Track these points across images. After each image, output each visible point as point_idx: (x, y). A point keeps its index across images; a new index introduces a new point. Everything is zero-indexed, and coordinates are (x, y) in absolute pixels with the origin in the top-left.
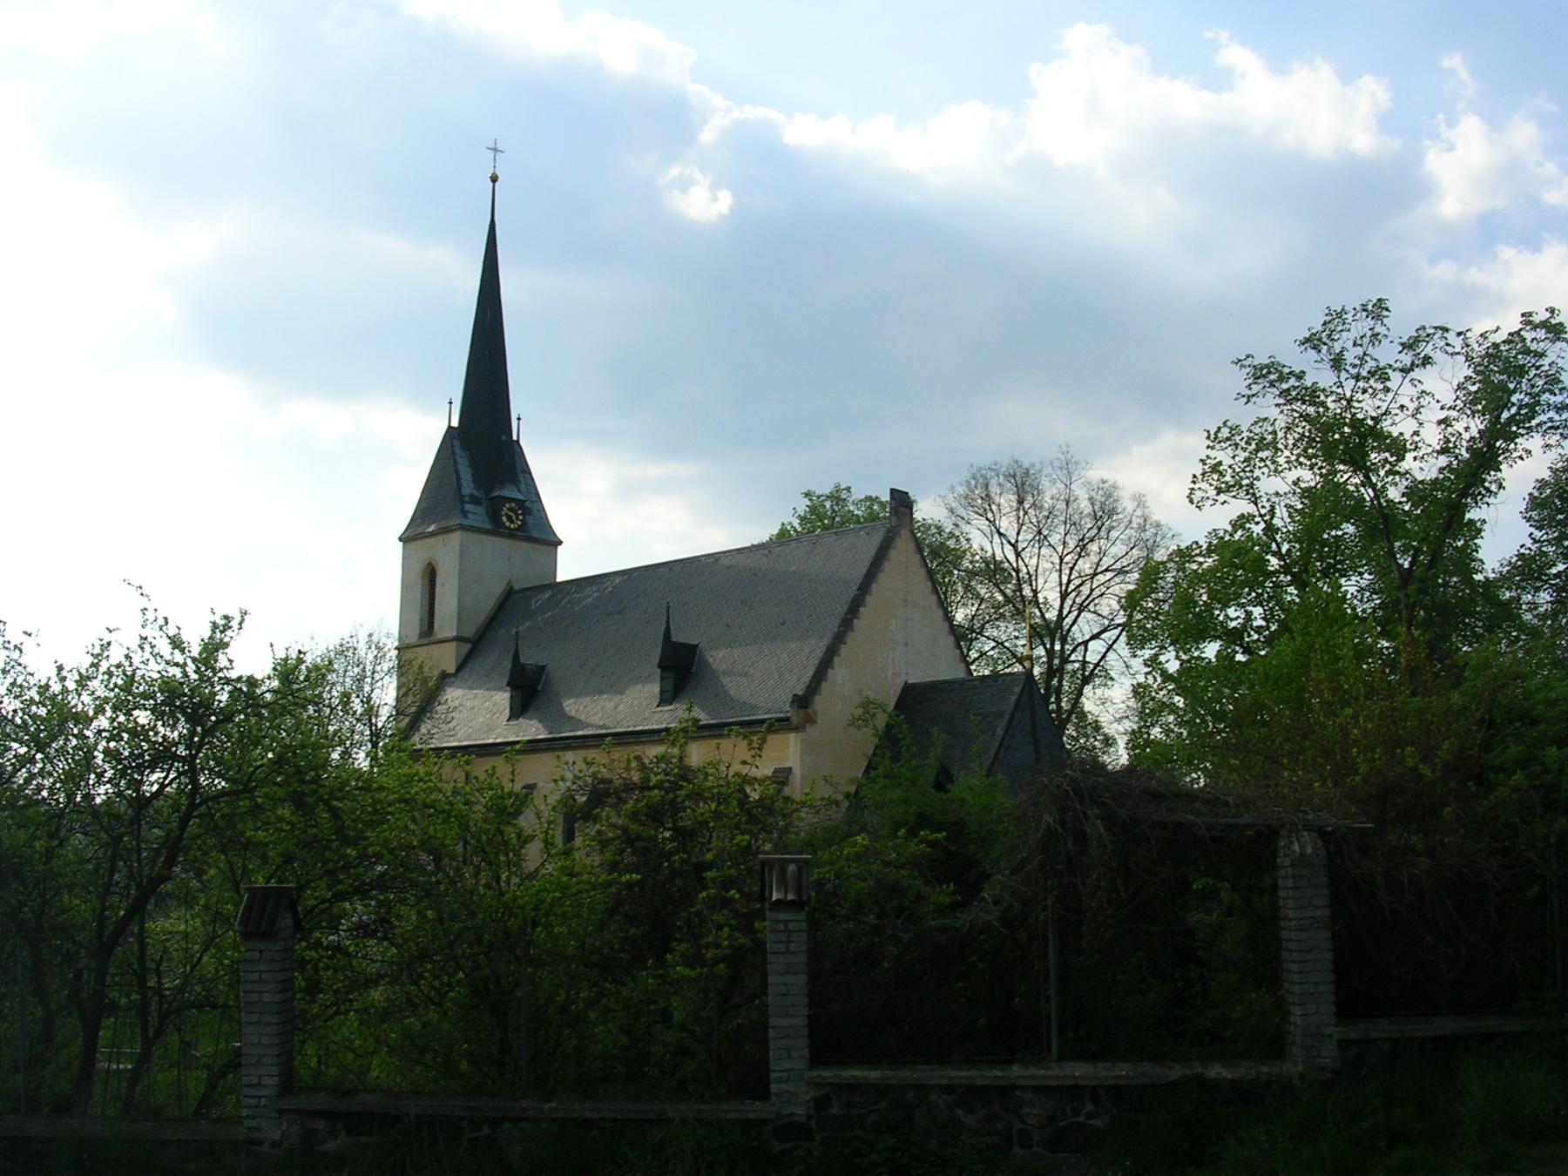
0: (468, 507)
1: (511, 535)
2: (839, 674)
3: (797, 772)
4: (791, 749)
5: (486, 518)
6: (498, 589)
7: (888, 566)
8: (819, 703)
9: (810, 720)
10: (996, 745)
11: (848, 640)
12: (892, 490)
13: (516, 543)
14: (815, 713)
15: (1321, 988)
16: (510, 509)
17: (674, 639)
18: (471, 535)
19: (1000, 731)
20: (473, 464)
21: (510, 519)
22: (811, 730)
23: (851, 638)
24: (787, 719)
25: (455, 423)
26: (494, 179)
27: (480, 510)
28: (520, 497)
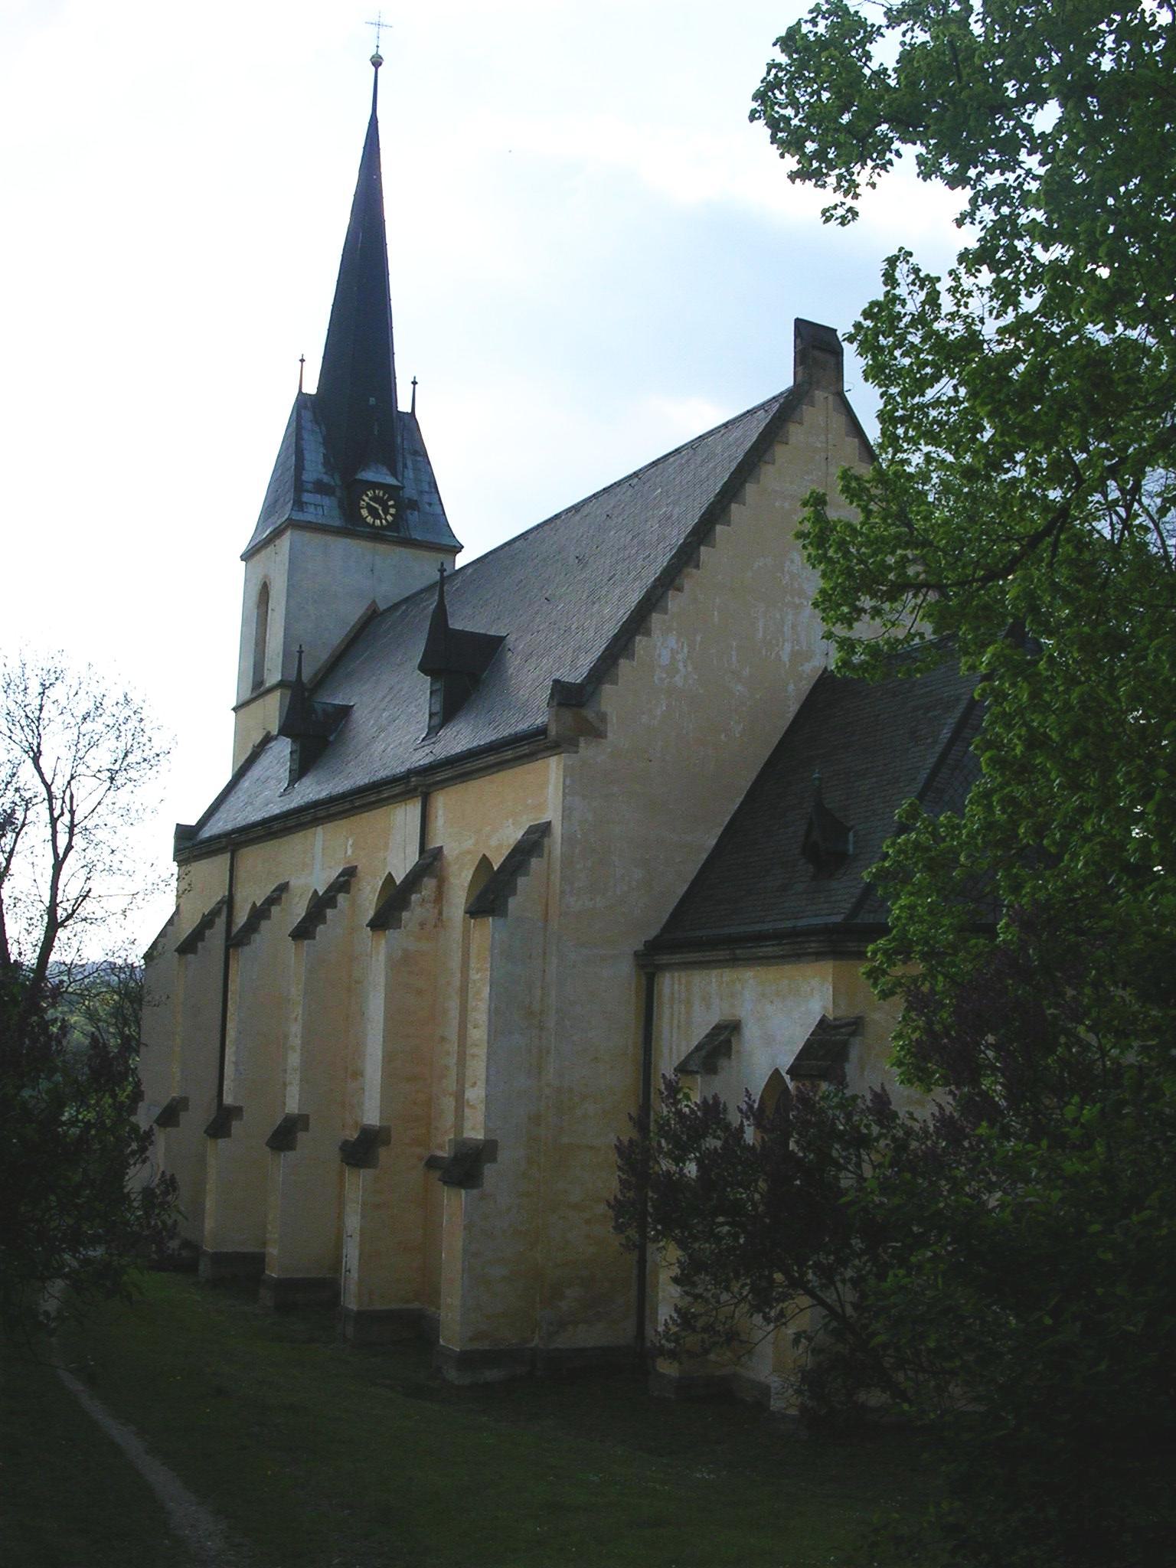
0: (307, 497)
1: (376, 535)
2: (663, 645)
3: (557, 829)
4: (551, 788)
5: (336, 512)
6: (354, 612)
7: (781, 452)
8: (611, 700)
9: (595, 732)
10: (932, 760)
11: (687, 584)
12: (799, 323)
13: (382, 548)
14: (603, 718)
15: (683, 981)
16: (375, 499)
17: (456, 624)
18: (307, 536)
19: (946, 734)
20: (327, 442)
21: (373, 512)
22: (587, 749)
23: (692, 580)
24: (542, 731)
25: (311, 387)
26: (377, 62)
27: (326, 501)
28: (391, 480)
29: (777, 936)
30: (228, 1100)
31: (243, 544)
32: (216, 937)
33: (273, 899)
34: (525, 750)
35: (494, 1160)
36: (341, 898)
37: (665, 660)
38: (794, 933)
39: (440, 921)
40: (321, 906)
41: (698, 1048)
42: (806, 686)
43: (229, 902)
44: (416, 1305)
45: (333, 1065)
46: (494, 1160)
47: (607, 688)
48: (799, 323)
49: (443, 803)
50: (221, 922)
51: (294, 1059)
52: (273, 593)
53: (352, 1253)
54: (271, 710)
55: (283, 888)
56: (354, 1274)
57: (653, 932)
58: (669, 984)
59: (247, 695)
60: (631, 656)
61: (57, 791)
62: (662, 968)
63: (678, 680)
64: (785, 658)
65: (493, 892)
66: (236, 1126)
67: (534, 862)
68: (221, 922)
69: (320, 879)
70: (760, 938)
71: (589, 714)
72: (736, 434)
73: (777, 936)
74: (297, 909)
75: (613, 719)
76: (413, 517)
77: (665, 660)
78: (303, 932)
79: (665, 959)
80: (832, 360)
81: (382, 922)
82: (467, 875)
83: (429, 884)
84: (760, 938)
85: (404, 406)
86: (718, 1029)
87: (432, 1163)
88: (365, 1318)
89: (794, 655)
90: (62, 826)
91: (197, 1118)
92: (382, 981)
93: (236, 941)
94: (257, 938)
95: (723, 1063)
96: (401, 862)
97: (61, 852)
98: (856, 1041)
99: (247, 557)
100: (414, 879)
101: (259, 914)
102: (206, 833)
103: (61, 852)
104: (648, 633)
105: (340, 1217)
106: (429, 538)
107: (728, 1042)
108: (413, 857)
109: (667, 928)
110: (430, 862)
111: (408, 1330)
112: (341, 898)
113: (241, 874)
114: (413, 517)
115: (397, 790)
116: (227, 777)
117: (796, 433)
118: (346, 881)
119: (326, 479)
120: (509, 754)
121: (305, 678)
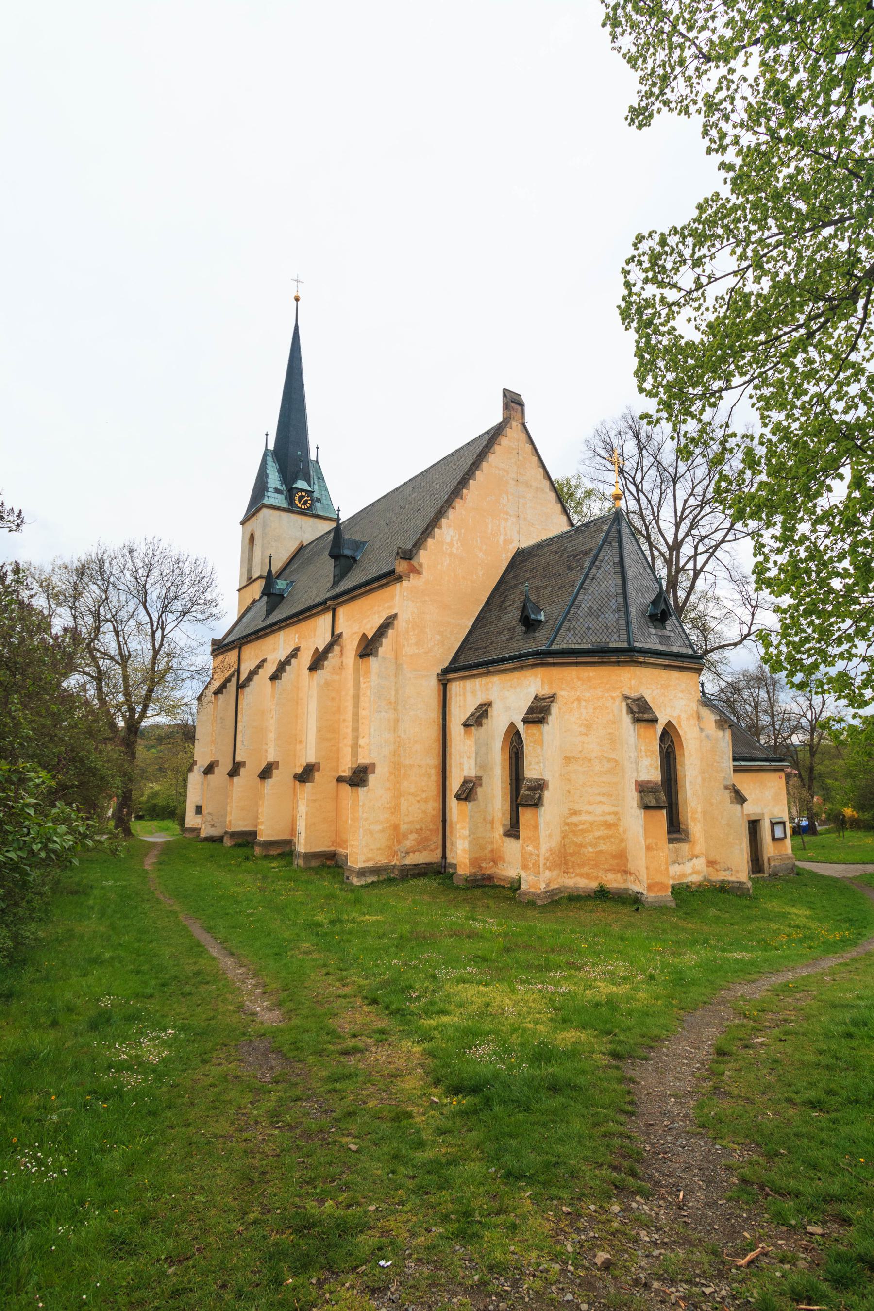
1: (302, 513)
5: (284, 501)
14: (421, 565)
28: (308, 488)
29: (511, 659)
30: (238, 759)
31: (241, 516)
32: (232, 686)
33: (259, 666)
34: (384, 581)
35: (374, 772)
36: (293, 660)
37: (448, 540)
38: (520, 657)
39: (342, 667)
40: (282, 667)
41: (472, 715)
42: (510, 556)
43: (238, 670)
44: (333, 849)
45: (291, 738)
46: (374, 772)
47: (422, 552)
48: (506, 392)
49: (342, 612)
50: (234, 679)
51: (272, 736)
52: (256, 537)
53: (301, 825)
54: (256, 590)
55: (264, 661)
56: (303, 835)
57: (446, 664)
58: (455, 688)
59: (245, 583)
60: (433, 538)
61: (155, 619)
62: (449, 681)
63: (454, 550)
64: (501, 541)
65: (368, 648)
66: (242, 770)
67: (390, 631)
68: (234, 679)
69: (282, 654)
70: (502, 660)
71: (414, 562)
72: (472, 447)
73: (511, 659)
74: (270, 668)
75: (425, 566)
76: (318, 505)
77: (448, 540)
78: (274, 677)
79: (451, 676)
80: (519, 408)
81: (315, 666)
82: (356, 643)
83: (336, 648)
84: (502, 660)
85: (313, 457)
86: (481, 705)
87: (340, 780)
88: (309, 856)
89: (505, 541)
90: (158, 634)
91: (225, 766)
92: (315, 695)
93: (241, 686)
94: (252, 684)
95: (484, 721)
96: (322, 640)
97: (157, 646)
98: (554, 704)
99: (243, 523)
100: (329, 648)
101: (253, 673)
102: (226, 642)
103: (157, 646)
104: (440, 528)
105: (295, 808)
106: (326, 514)
107: (487, 711)
108: (328, 638)
109: (452, 662)
110: (336, 639)
111: (330, 863)
112: (293, 660)
113: (243, 656)
114: (318, 505)
115: (320, 608)
116: (236, 618)
117: (504, 441)
118: (294, 654)
119: (279, 487)
120: (376, 585)
121: (274, 571)
